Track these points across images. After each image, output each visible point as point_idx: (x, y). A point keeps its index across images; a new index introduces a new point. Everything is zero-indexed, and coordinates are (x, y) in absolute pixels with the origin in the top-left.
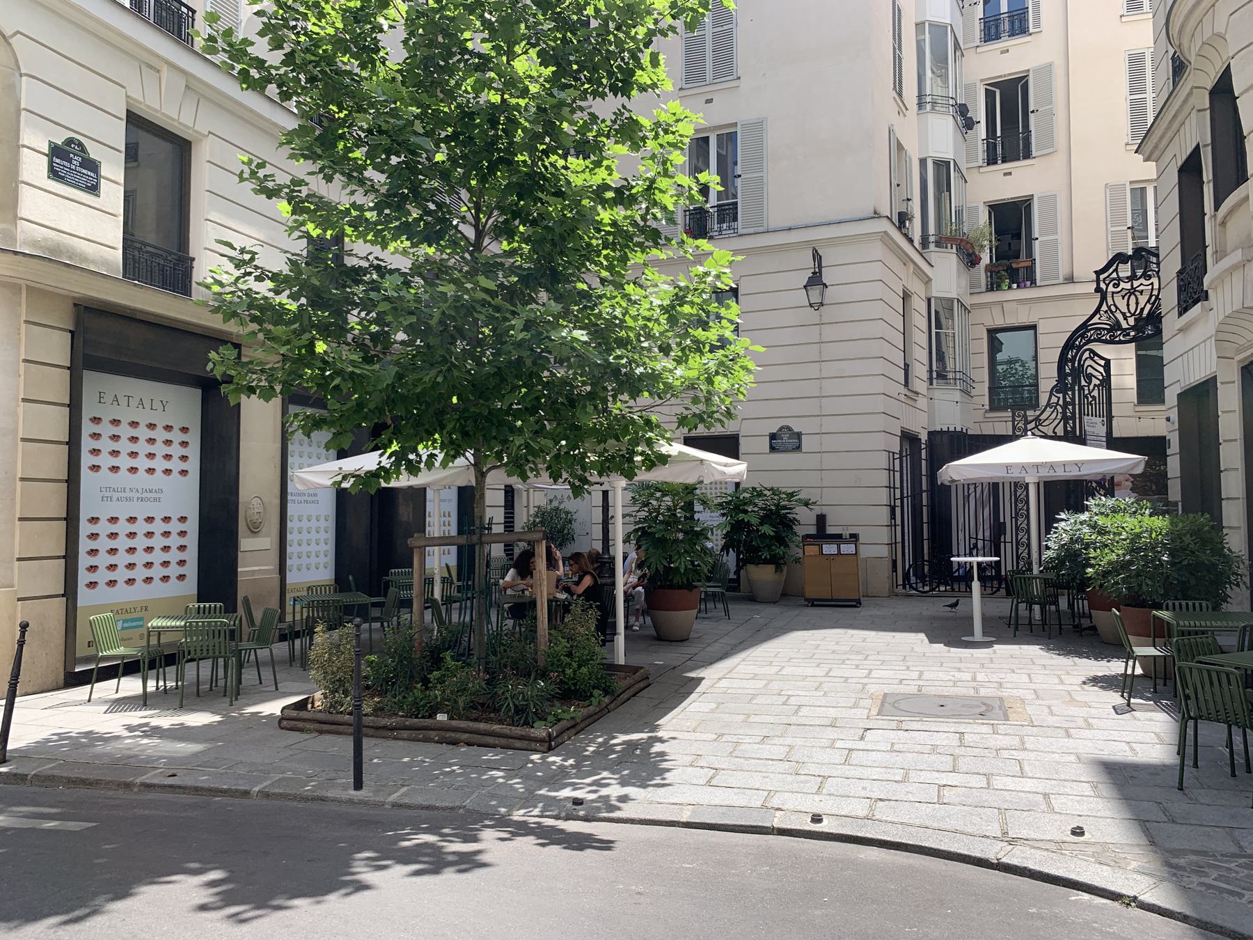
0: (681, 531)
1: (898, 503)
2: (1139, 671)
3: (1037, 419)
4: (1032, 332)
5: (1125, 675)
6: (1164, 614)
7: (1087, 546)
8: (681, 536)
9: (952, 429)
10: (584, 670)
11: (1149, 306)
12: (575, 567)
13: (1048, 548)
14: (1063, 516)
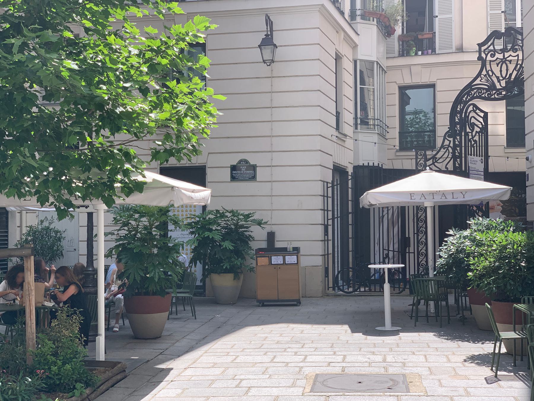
0: (156, 246)
1: (330, 222)
2: (504, 350)
3: (434, 157)
4: (432, 89)
5: (494, 353)
6: (521, 307)
7: (468, 256)
8: (155, 251)
9: (371, 164)
10: (68, 366)
11: (515, 73)
12: (62, 279)
13: (440, 257)
14: (451, 232)
